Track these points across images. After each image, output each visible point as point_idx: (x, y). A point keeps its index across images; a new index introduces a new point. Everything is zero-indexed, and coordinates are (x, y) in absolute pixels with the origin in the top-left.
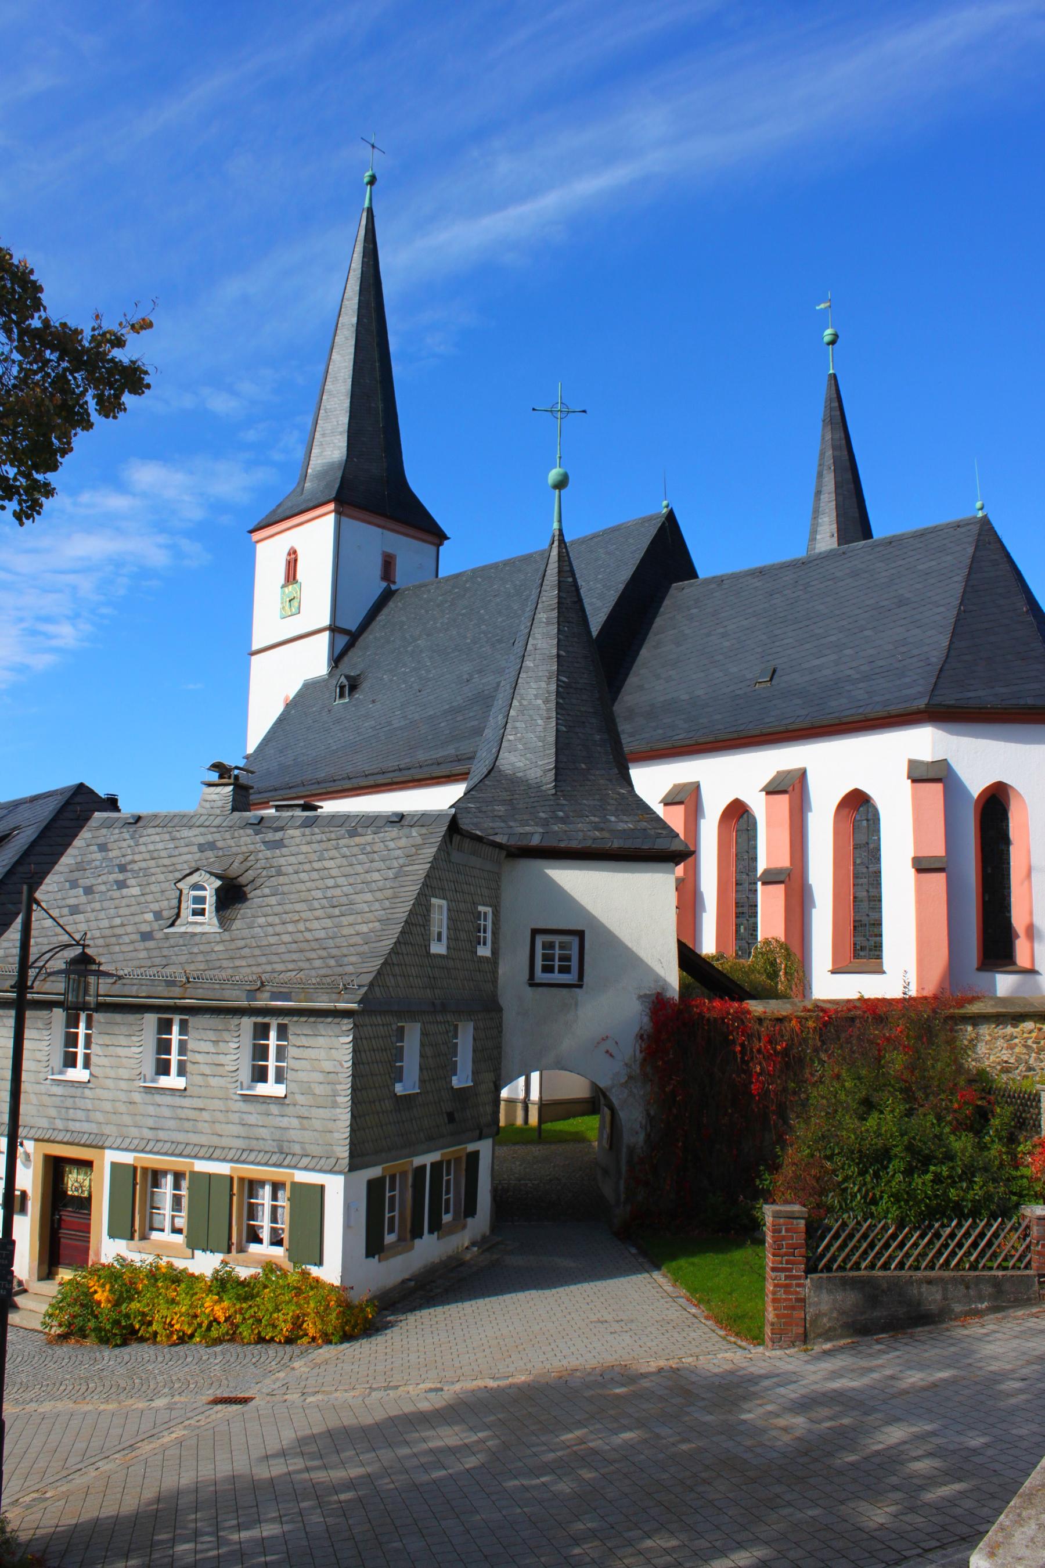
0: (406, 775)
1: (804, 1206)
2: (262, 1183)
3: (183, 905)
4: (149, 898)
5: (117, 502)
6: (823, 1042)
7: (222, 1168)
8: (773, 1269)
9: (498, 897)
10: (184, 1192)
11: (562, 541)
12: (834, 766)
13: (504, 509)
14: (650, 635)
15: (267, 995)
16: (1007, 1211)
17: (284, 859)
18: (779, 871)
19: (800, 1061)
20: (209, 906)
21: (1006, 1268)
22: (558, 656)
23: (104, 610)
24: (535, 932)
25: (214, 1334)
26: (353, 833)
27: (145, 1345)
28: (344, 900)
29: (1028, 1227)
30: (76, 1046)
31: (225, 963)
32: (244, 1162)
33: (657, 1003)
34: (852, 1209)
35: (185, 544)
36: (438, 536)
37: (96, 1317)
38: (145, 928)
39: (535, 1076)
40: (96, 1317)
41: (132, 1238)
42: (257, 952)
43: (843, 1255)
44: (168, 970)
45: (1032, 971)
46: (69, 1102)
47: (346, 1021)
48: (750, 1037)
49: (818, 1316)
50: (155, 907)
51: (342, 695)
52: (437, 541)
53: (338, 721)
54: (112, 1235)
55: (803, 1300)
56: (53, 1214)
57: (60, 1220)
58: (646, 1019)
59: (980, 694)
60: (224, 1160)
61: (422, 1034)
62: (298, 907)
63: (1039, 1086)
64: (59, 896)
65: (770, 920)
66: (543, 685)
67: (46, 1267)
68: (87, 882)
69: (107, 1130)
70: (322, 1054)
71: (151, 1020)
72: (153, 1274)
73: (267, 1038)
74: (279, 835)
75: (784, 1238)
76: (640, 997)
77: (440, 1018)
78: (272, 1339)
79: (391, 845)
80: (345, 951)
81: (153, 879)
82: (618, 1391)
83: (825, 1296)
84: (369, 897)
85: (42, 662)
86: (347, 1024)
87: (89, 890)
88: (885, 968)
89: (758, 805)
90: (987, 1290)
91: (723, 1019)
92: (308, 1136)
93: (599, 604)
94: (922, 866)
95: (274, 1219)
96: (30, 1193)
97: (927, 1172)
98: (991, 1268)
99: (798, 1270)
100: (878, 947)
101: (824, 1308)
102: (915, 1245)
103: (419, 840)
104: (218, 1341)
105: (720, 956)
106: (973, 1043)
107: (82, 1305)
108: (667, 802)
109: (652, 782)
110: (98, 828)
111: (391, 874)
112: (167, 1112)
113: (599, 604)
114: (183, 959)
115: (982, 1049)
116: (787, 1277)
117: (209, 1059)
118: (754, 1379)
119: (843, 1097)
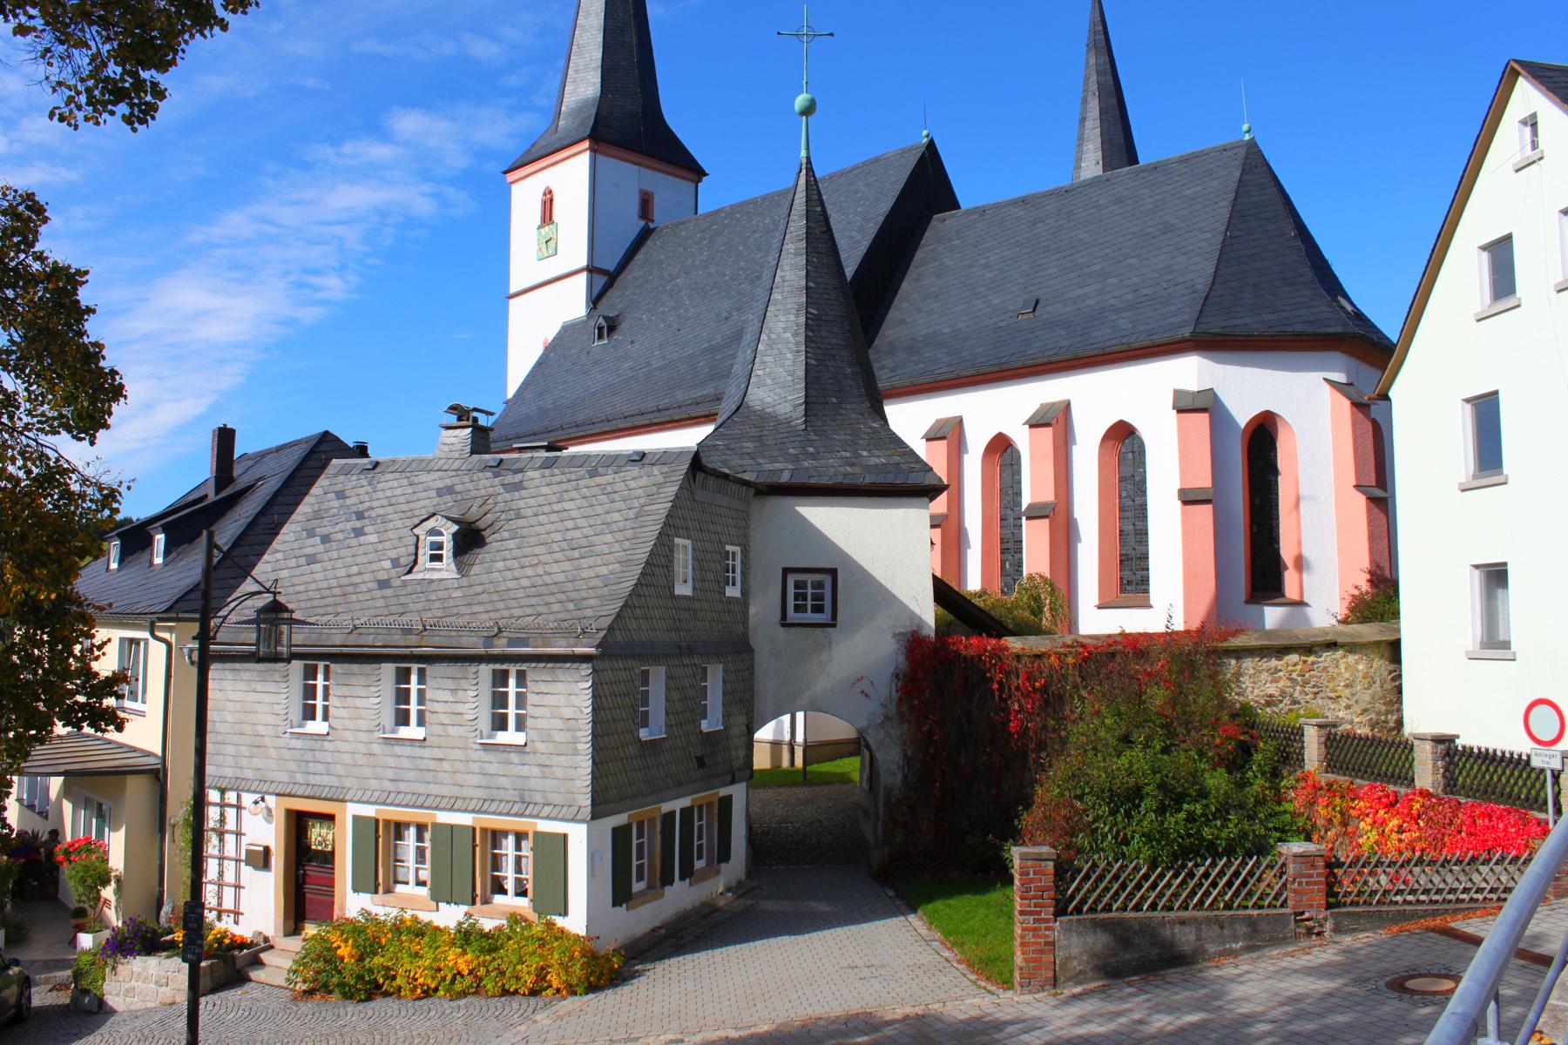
0: (665, 417)
1: (1054, 847)
2: (505, 833)
3: (421, 551)
4: (387, 545)
5: (381, 152)
6: (1083, 679)
7: (465, 819)
8: (1021, 913)
9: (746, 536)
10: (427, 844)
11: (810, 170)
12: (1099, 397)
13: (756, 142)
14: (911, 267)
15: (504, 641)
16: (1261, 849)
17: (523, 502)
18: (1044, 506)
19: (1060, 698)
20: (447, 552)
21: (1261, 907)
22: (807, 288)
23: (371, 261)
24: (786, 571)
25: (458, 987)
26: (593, 474)
27: (390, 999)
28: (584, 542)
29: (1284, 865)
30: (408, 703)
31: (463, 610)
32: (485, 812)
33: (914, 643)
34: (1103, 850)
35: (451, 192)
36: (694, 171)
37: (340, 972)
38: (383, 576)
39: (800, 716)
40: (340, 972)
41: (376, 892)
42: (495, 597)
43: (1095, 894)
44: (405, 618)
45: (1301, 603)
46: (309, 756)
47: (584, 666)
48: (1008, 674)
49: (1068, 959)
50: (393, 554)
51: (600, 337)
52: (693, 176)
53: (597, 363)
54: (356, 890)
55: (1053, 944)
56: (297, 870)
57: (305, 874)
58: (902, 658)
59: (1246, 321)
60: (465, 811)
61: (667, 677)
62: (537, 550)
63: (1302, 720)
64: (296, 545)
65: (1036, 557)
66: (792, 318)
67: (291, 924)
68: (325, 531)
69: (348, 783)
70: (561, 700)
71: (389, 669)
72: (397, 928)
73: (506, 686)
74: (518, 477)
75: (1032, 880)
76: (895, 635)
77: (686, 661)
78: (516, 992)
79: (633, 484)
80: (584, 594)
81: (391, 525)
82: (860, 1040)
83: (1075, 939)
84: (609, 538)
85: (310, 315)
86: (586, 669)
87: (326, 539)
88: (1152, 602)
89: (1022, 438)
90: (1242, 929)
91: (980, 657)
92: (549, 784)
93: (858, 237)
94: (1189, 498)
95: (518, 870)
96: (273, 849)
97: (1179, 810)
98: (1246, 907)
99: (1047, 913)
100: (1145, 581)
101: (1075, 951)
102: (1169, 885)
103: (660, 479)
104: (463, 994)
105: (982, 593)
106: (1238, 675)
107: (326, 961)
108: (931, 437)
109: (910, 420)
110: (335, 475)
111: (631, 514)
112: (406, 763)
113: (858, 237)
114: (420, 606)
115: (1246, 682)
116: (1035, 921)
117: (448, 708)
118: (1000, 1026)
119: (1102, 734)
